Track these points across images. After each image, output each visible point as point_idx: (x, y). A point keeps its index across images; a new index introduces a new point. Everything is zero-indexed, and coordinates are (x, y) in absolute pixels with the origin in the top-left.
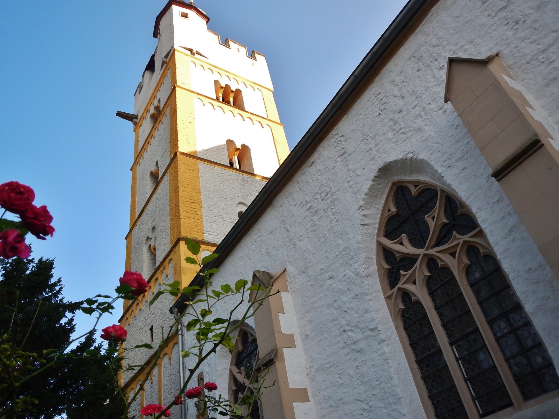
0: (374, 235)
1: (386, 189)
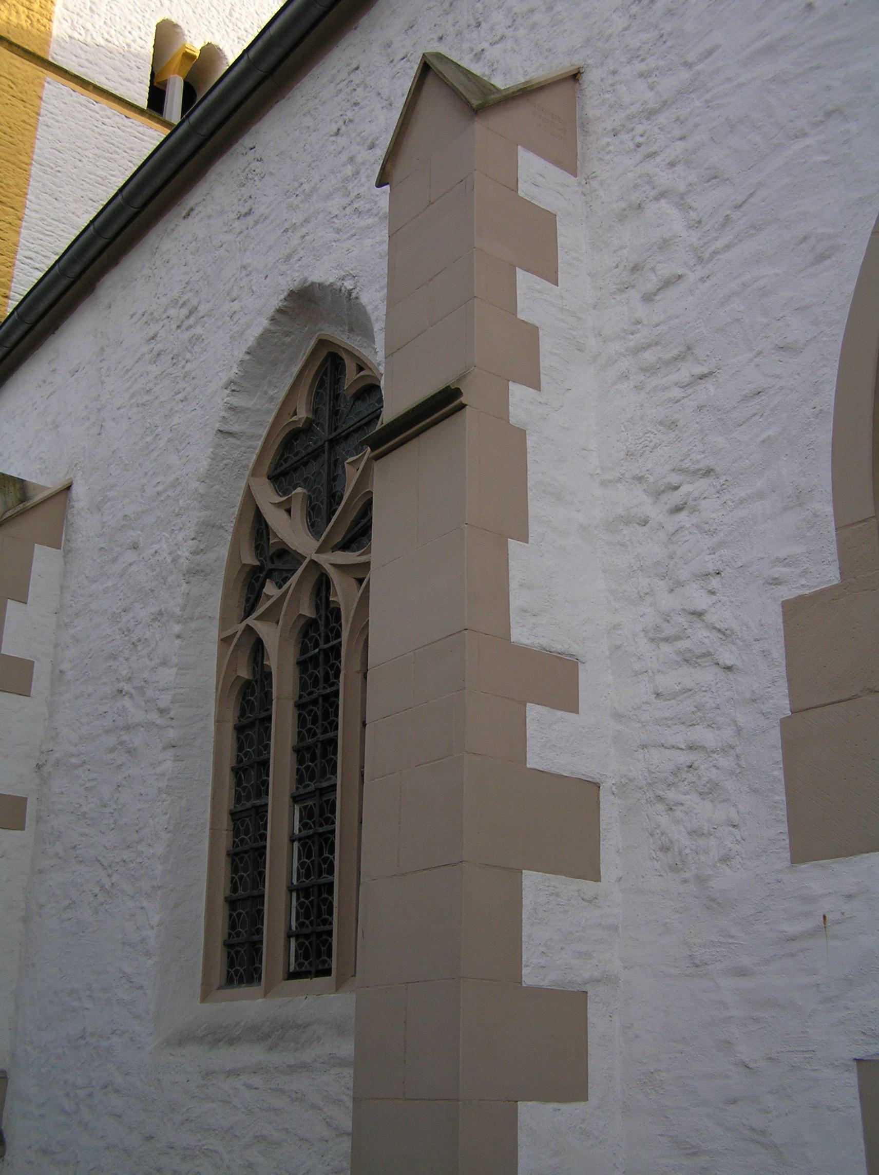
0: (247, 466)
1: (303, 352)
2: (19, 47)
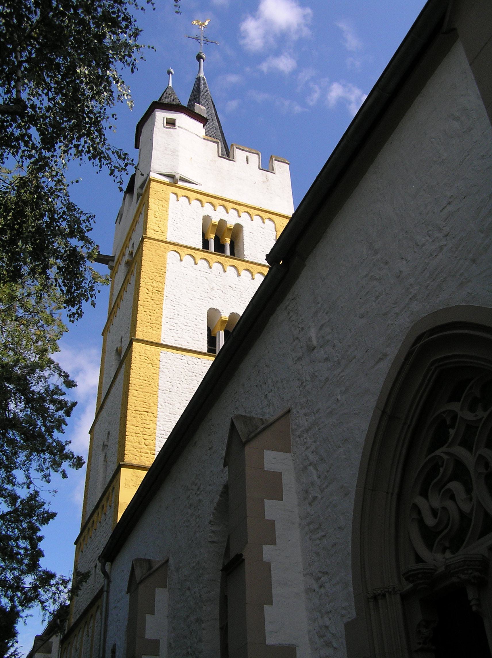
2: (148, 341)
